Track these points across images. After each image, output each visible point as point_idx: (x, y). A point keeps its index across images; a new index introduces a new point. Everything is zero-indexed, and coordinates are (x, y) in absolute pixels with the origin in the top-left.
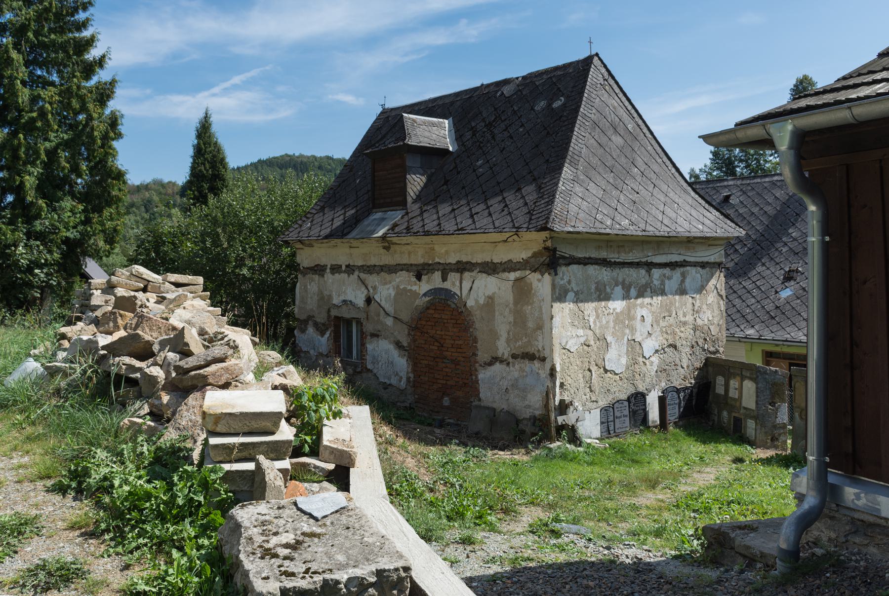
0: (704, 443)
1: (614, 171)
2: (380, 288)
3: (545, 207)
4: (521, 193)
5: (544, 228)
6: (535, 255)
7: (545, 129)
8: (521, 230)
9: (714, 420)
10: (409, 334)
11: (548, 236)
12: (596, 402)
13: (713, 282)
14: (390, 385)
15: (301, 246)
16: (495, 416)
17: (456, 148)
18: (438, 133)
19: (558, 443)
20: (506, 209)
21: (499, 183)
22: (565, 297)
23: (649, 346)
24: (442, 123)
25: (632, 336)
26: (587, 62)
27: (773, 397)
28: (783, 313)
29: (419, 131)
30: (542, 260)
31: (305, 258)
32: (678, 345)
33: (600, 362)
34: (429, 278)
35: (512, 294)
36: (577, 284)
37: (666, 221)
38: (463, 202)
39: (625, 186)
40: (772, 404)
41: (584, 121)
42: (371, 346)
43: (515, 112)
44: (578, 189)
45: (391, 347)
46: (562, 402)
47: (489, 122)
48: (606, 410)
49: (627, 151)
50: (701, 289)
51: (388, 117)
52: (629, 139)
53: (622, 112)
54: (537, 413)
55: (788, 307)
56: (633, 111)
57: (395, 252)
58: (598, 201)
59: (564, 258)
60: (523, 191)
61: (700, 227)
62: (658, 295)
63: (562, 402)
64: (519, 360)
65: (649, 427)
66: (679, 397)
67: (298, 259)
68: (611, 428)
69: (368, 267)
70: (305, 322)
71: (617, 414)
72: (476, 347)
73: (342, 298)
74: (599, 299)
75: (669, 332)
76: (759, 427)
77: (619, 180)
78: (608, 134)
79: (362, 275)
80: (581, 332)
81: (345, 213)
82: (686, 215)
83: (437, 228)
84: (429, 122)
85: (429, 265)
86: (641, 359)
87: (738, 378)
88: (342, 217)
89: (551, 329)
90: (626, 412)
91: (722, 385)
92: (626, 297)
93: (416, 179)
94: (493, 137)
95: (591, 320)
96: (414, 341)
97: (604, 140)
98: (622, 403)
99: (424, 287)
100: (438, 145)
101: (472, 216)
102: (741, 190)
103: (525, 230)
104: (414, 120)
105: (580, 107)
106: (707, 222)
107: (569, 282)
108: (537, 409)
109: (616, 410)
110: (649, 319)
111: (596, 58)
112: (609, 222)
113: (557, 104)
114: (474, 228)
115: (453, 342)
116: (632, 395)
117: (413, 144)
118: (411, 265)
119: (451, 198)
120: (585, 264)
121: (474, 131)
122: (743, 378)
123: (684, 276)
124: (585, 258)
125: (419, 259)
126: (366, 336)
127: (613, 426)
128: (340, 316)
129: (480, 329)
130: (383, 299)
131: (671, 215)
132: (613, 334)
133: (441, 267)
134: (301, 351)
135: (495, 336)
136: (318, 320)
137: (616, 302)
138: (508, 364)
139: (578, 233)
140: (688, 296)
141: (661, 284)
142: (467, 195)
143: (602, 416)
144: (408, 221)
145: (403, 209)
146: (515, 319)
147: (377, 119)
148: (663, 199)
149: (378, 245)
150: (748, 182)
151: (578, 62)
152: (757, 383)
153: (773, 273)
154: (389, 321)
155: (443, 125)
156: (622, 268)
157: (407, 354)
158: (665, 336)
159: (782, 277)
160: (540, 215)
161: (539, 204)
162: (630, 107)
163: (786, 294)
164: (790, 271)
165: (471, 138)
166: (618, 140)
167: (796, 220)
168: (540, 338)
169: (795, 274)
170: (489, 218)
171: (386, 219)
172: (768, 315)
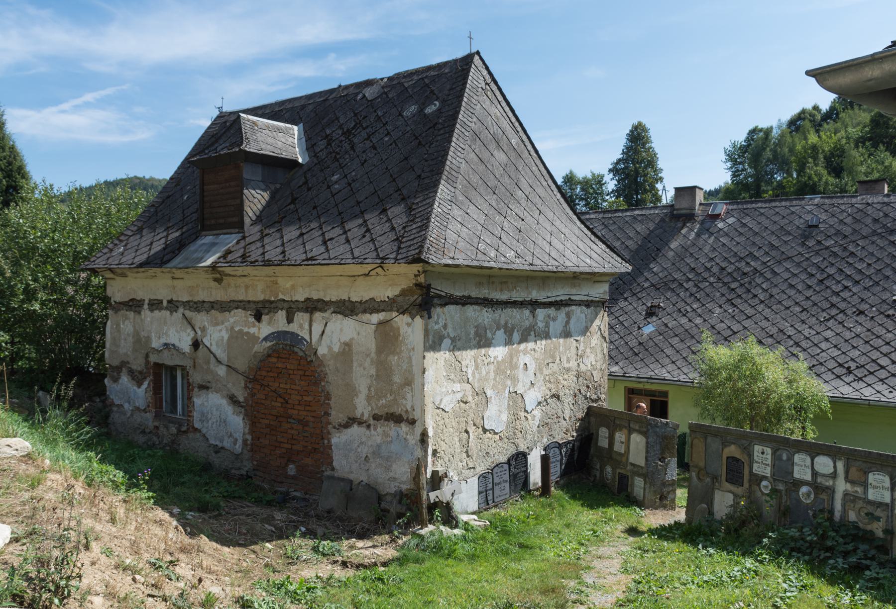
0: (591, 507)
1: (496, 192)
2: (211, 330)
3: (418, 232)
4: (387, 216)
5: (417, 260)
6: (403, 293)
7: (417, 138)
8: (387, 261)
9: (595, 476)
10: (246, 387)
11: (421, 269)
12: (474, 468)
13: (597, 322)
14: (222, 448)
15: (112, 276)
16: (351, 490)
17: (307, 159)
18: (284, 141)
19: (431, 527)
20: (368, 235)
21: (358, 203)
22: (440, 345)
23: (532, 397)
24: (290, 129)
25: (514, 388)
26: (466, 62)
27: (663, 452)
28: (647, 350)
29: (260, 136)
30: (412, 299)
31: (118, 291)
32: (561, 394)
33: (478, 421)
34: (271, 319)
35: (374, 340)
36: (454, 329)
37: (553, 254)
38: (314, 225)
39: (509, 211)
40: (662, 459)
41: (463, 130)
42: (199, 400)
43: (379, 118)
44: (456, 212)
45: (224, 402)
46: (435, 473)
47: (348, 130)
48: (484, 477)
49: (511, 170)
50: (585, 331)
51: (225, 122)
52: (513, 155)
53: (505, 124)
54: (404, 487)
55: (651, 343)
56: (517, 124)
57: (229, 285)
58: (480, 228)
59: (439, 297)
60: (389, 212)
61: (588, 261)
62: (542, 339)
63: (435, 473)
64: (382, 421)
65: (530, 491)
66: (561, 453)
67: (109, 292)
68: (490, 498)
69: (195, 303)
70: (118, 369)
71: (497, 480)
72: (329, 404)
73: (163, 340)
74: (479, 346)
75: (552, 381)
76: (648, 486)
77: (503, 204)
78: (491, 148)
79: (189, 314)
80: (457, 387)
81: (167, 236)
82: (573, 247)
83: (280, 257)
84: (273, 126)
85: (271, 302)
86: (523, 414)
87: (625, 431)
88: (163, 240)
89: (423, 385)
90: (506, 477)
91: (606, 438)
92: (508, 342)
93: (256, 195)
94: (352, 148)
95: (470, 372)
96: (253, 395)
97: (485, 155)
98: (502, 467)
99: (265, 329)
100: (284, 155)
101: (325, 243)
102: (603, 224)
103: (393, 261)
104: (254, 123)
105: (458, 113)
106: (594, 256)
107: (445, 326)
108: (404, 483)
109: (495, 475)
110: (532, 368)
111: (476, 57)
112: (493, 254)
113: (430, 110)
114: (327, 257)
115: (300, 398)
116: (513, 456)
117: (252, 150)
118: (249, 302)
119: (299, 219)
120: (464, 304)
121: (329, 139)
122: (631, 431)
123: (568, 316)
124: (464, 296)
125: (258, 294)
126: (193, 388)
127: (491, 495)
128: (161, 362)
129: (334, 383)
130: (214, 343)
131: (558, 247)
132: (494, 387)
133: (286, 305)
134: (112, 404)
135: (352, 391)
136: (134, 367)
137: (498, 348)
138: (369, 427)
139: (457, 266)
140: (572, 339)
141: (545, 327)
142: (319, 217)
143: (480, 484)
144: (244, 248)
145: (239, 233)
146: (377, 371)
147: (212, 124)
148: (549, 228)
149: (208, 276)
150: (610, 215)
151: (455, 61)
152: (647, 438)
153: (635, 308)
154: (222, 371)
155: (291, 132)
156: (505, 308)
157: (243, 410)
158: (548, 385)
159: (644, 313)
160: (412, 243)
161: (409, 228)
162: (513, 119)
163: (648, 329)
164: (652, 306)
165: (326, 148)
166: (501, 156)
167: (657, 255)
168: (409, 396)
169: (657, 310)
170: (347, 245)
171: (217, 243)
172: (631, 352)
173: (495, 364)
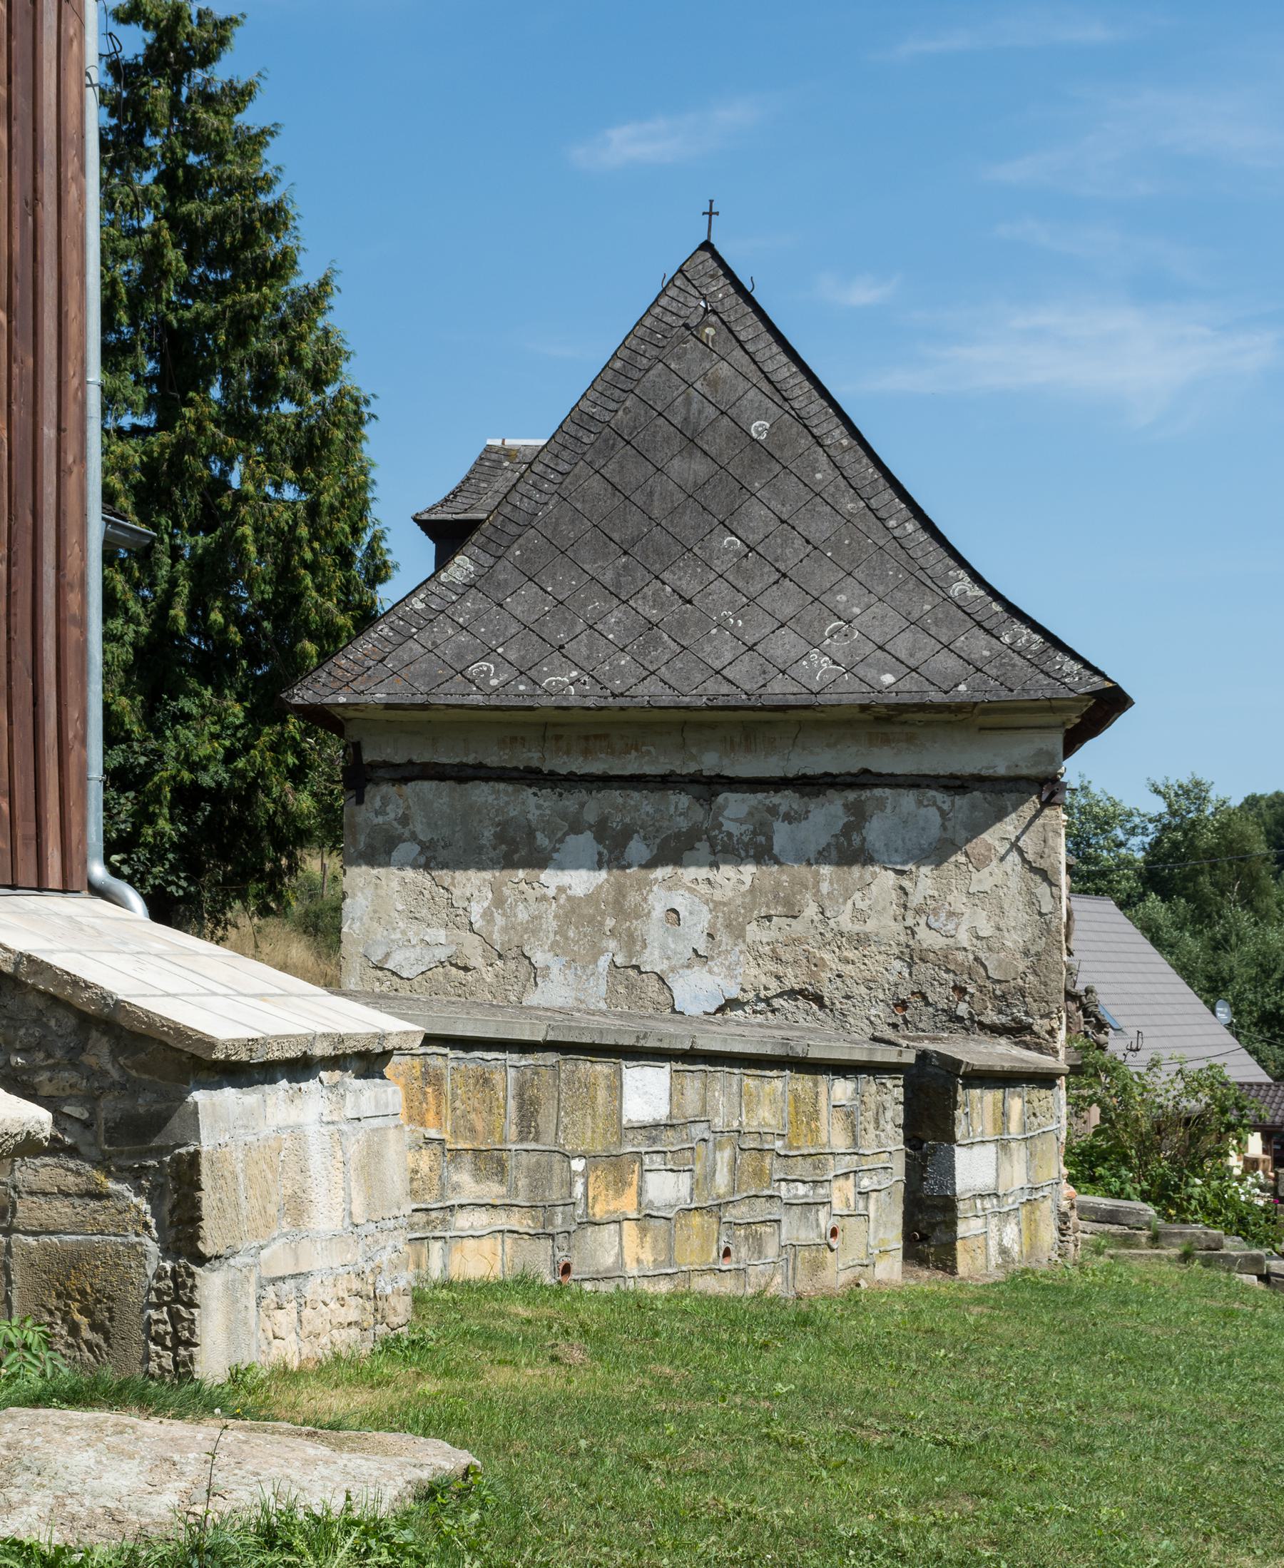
74: (509, 863)
80: (440, 935)
107: (405, 820)
156: (599, 790)
173: (562, 900)
